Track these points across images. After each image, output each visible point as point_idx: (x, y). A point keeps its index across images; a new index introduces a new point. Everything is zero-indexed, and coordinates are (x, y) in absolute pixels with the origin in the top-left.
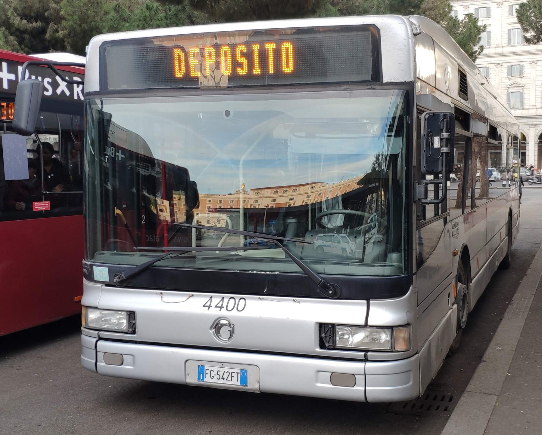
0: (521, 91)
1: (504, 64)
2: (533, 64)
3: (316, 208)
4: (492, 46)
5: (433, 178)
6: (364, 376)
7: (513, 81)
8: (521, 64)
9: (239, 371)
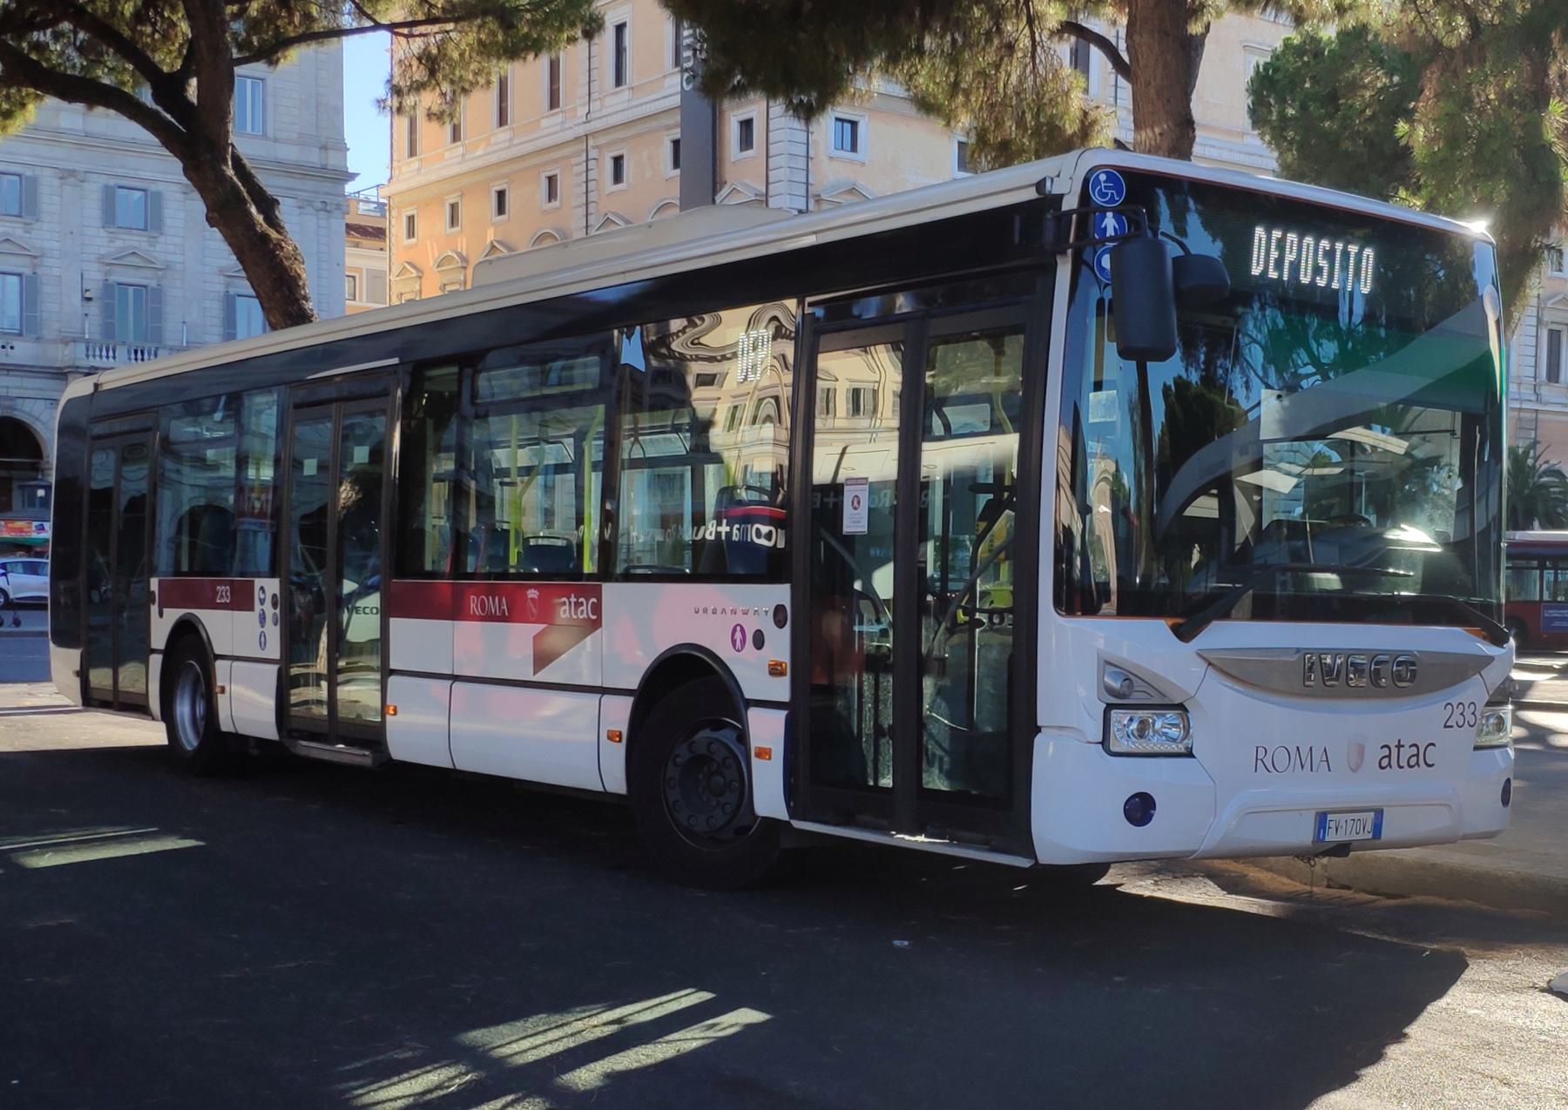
0: (153, 284)
8: (153, 187)
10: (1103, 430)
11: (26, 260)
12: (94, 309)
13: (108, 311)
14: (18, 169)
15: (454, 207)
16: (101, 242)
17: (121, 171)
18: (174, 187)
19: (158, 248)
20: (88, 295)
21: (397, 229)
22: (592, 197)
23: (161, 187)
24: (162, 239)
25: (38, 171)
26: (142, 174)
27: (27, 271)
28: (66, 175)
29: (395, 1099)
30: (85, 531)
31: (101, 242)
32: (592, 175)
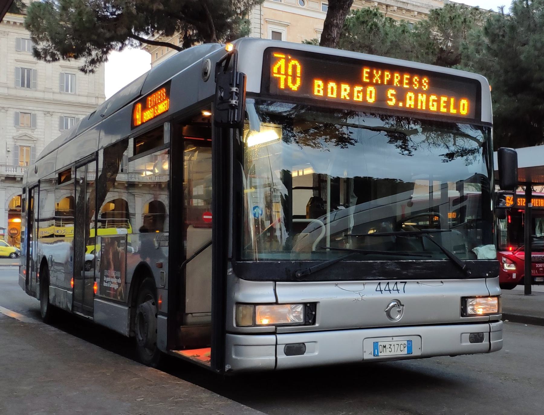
0: (33, 145)
1: (54, 113)
2: (48, 115)
3: (255, 219)
4: (39, 88)
5: (495, 170)
6: (275, 346)
7: (22, 132)
8: (33, 112)
9: (406, 342)
12: (11, 155)
13: (16, 155)
14: (73, 116)
16: (14, 132)
17: (21, 107)
18: (41, 112)
19: (35, 133)
20: (8, 150)
24: (36, 130)
25: (36, 112)
31: (14, 132)
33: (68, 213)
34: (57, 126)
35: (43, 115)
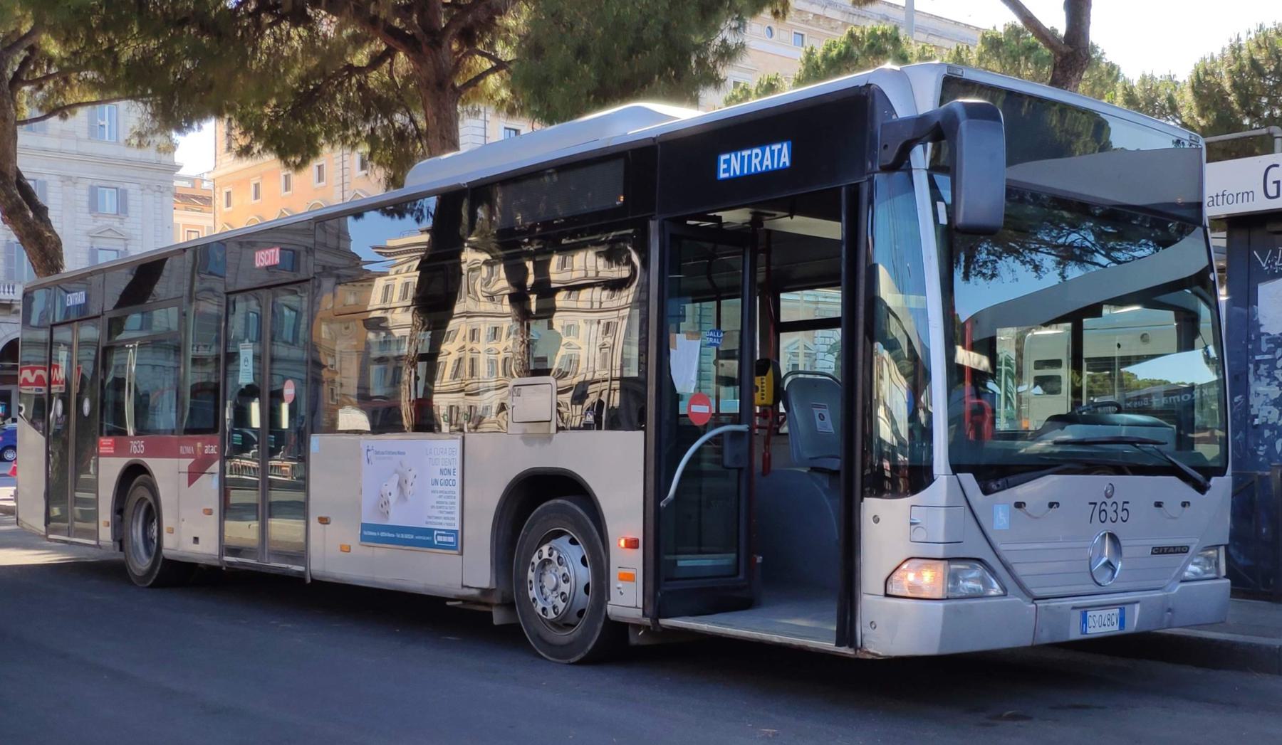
7: (103, 222)
8: (121, 186)
10: (1218, 249)
11: (122, 242)
14: (115, 185)
15: (257, 186)
18: (54, 178)
21: (220, 201)
22: (346, 179)
23: (46, 178)
25: (127, 186)
26: (34, 170)
27: (122, 249)
28: (67, 179)
29: (56, 541)
30: (843, 270)
32: (346, 165)
33: (153, 544)
34: (85, 204)
35: (60, 184)
